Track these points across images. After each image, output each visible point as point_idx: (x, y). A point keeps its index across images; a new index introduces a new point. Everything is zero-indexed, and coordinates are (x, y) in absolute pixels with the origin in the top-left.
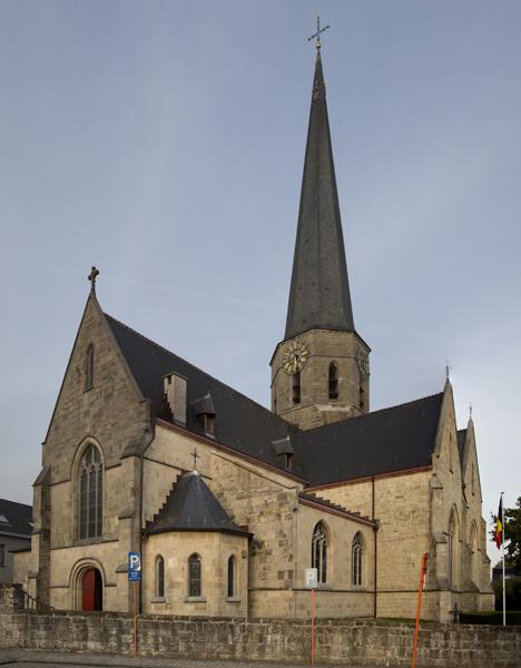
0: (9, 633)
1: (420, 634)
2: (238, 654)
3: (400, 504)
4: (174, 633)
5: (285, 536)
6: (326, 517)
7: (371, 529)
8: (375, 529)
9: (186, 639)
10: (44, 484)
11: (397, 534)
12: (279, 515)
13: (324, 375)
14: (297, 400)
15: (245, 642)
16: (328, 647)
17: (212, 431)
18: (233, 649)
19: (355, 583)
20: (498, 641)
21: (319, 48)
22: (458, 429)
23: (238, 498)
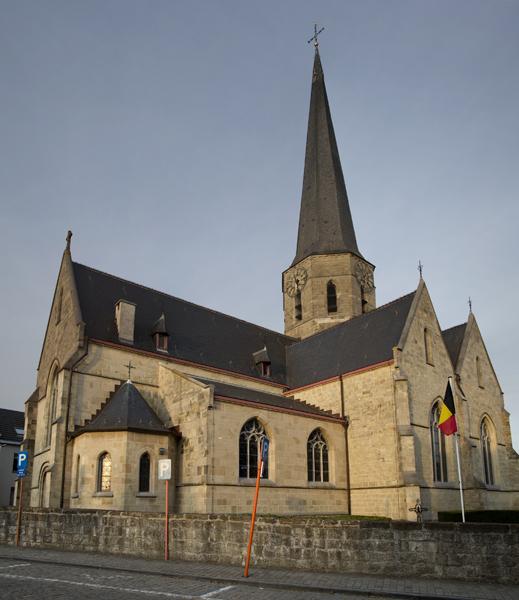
1: (278, 530)
2: (101, 547)
3: (367, 399)
4: (49, 525)
6: (262, 415)
7: (341, 426)
8: (346, 425)
9: (58, 530)
10: (33, 402)
11: (366, 429)
12: (198, 414)
13: (322, 293)
14: (299, 317)
15: (107, 534)
16: (182, 542)
17: (166, 346)
18: (96, 541)
19: (439, 479)
20: (371, 539)
22: (443, 329)
23: (174, 402)
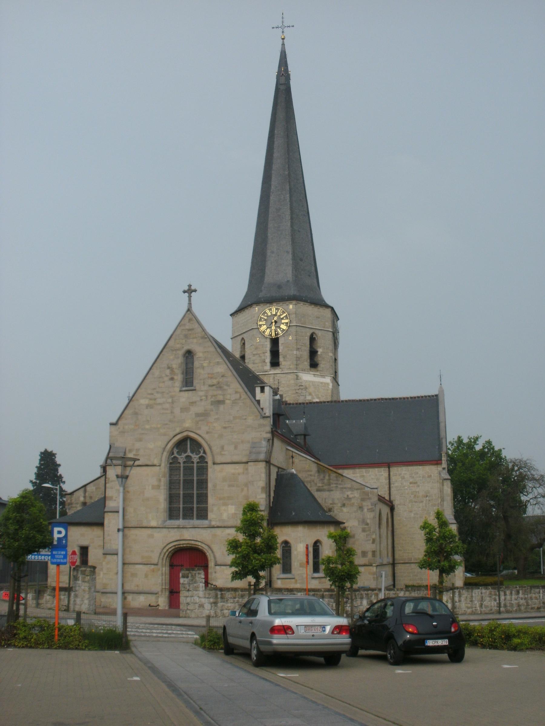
0: (201, 606)
5: (367, 524)
12: (361, 508)
21: (283, 39)
